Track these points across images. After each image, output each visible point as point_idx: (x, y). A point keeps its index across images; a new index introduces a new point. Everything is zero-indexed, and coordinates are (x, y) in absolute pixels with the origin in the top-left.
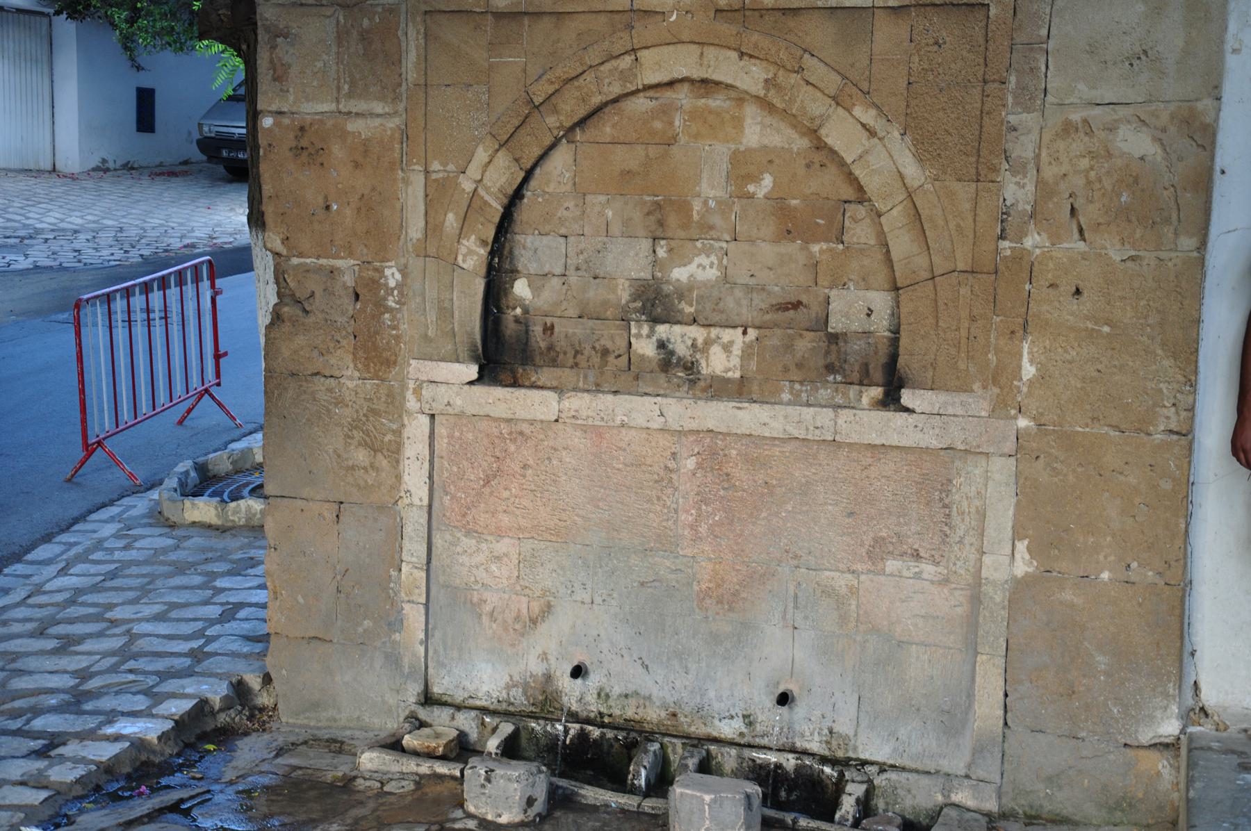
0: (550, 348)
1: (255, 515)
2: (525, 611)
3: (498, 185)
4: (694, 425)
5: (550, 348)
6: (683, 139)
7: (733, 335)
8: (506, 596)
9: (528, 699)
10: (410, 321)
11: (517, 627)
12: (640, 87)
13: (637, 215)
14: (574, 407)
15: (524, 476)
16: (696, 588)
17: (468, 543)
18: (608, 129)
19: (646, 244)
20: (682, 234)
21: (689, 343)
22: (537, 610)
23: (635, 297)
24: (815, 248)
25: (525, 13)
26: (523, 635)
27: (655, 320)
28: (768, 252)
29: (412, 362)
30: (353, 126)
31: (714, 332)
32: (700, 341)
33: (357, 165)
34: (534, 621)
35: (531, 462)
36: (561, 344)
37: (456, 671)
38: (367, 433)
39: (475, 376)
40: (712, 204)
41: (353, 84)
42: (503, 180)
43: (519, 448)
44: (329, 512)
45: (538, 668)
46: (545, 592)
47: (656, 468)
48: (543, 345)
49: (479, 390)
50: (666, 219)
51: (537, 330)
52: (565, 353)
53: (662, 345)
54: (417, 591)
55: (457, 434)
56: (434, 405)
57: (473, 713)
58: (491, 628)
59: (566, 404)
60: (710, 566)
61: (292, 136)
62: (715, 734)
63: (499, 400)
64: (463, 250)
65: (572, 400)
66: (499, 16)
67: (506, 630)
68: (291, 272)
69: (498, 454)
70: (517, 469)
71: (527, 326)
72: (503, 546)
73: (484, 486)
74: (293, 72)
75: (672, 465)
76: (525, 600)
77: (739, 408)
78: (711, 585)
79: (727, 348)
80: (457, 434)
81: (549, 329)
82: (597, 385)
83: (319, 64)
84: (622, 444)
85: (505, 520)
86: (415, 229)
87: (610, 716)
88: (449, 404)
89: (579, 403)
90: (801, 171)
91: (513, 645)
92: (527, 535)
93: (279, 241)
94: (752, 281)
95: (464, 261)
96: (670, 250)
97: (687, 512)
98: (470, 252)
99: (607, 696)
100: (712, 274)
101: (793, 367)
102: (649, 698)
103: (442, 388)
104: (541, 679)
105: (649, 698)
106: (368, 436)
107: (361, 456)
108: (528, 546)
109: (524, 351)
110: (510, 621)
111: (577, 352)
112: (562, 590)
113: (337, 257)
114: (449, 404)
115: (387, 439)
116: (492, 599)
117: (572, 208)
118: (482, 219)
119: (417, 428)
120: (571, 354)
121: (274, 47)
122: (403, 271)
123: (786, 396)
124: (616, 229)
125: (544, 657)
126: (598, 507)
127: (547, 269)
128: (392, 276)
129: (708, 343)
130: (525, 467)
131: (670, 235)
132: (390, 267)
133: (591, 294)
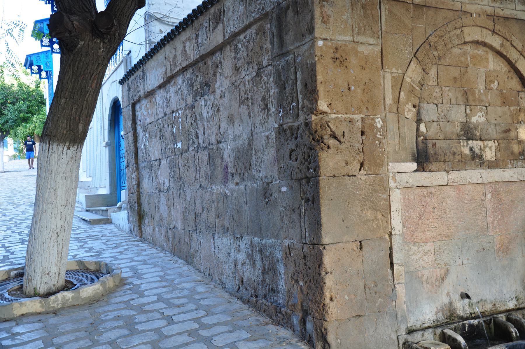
0: (436, 153)
1: (68, 300)
2: (439, 275)
3: (418, 80)
4: (491, 180)
5: (436, 153)
6: (470, 66)
7: (491, 143)
8: (431, 270)
9: (444, 317)
10: (391, 144)
11: (437, 283)
12: (142, 94)
13: (460, 95)
14: (453, 177)
15: (434, 212)
16: (495, 248)
17: (414, 248)
18: (448, 60)
19: (463, 107)
20: (474, 104)
21: (479, 148)
22: (443, 274)
23: (462, 129)
24: (512, 109)
25: (425, 6)
26: (439, 287)
27: (468, 139)
28: (500, 110)
29: (390, 164)
30: (361, 48)
31: (486, 142)
32: (482, 147)
33: (363, 68)
34: (443, 279)
35: (436, 206)
36: (439, 152)
37: (416, 313)
38: (372, 202)
39: (416, 168)
40: (482, 91)
41: (359, 29)
42: (420, 78)
43: (431, 199)
44: (355, 246)
45: (446, 300)
46: (446, 264)
47: (478, 201)
48: (432, 152)
49: (417, 174)
50: (468, 98)
51: (430, 145)
52: (441, 155)
53: (471, 149)
54: (401, 277)
55: (407, 197)
56: (401, 183)
57: (430, 330)
58: (427, 287)
59: (450, 176)
60: (499, 238)
61: (331, 51)
62: (508, 308)
63: (424, 178)
64: (407, 110)
65: (452, 174)
66: (416, 5)
67: (433, 286)
68: (332, 122)
69: (423, 204)
70: (431, 210)
71: (426, 144)
72: (429, 247)
73: (419, 220)
74: (332, 19)
75: (483, 198)
76: (438, 270)
77: (504, 171)
78: (500, 246)
79: (490, 148)
80: (407, 197)
81: (434, 145)
82: (452, 168)
83: (344, 17)
84: (467, 192)
85: (428, 234)
86: (389, 100)
87: (474, 313)
88: (407, 182)
89: (454, 176)
90: (506, 80)
91: (436, 293)
92: (437, 239)
93: (326, 106)
94: (496, 122)
95: (407, 114)
96: (471, 110)
97: (490, 217)
98: (410, 110)
99: (472, 304)
100: (483, 119)
101: (510, 155)
102: (486, 301)
103: (404, 175)
104: (448, 305)
105: (486, 301)
106: (374, 203)
107: (369, 214)
108: (437, 244)
109: (426, 155)
110: (434, 282)
111: (445, 154)
112: (452, 262)
113: (354, 113)
114: (407, 182)
115: (382, 203)
116: (426, 273)
117: (438, 92)
118: (413, 95)
119: (396, 196)
120: (442, 156)
121: (322, 6)
122: (384, 121)
123: (510, 166)
124: (453, 101)
125: (448, 294)
126: (461, 221)
127: (432, 119)
128: (379, 123)
129: (485, 147)
130: (434, 208)
131: (470, 104)
132: (377, 118)
133: (447, 129)
